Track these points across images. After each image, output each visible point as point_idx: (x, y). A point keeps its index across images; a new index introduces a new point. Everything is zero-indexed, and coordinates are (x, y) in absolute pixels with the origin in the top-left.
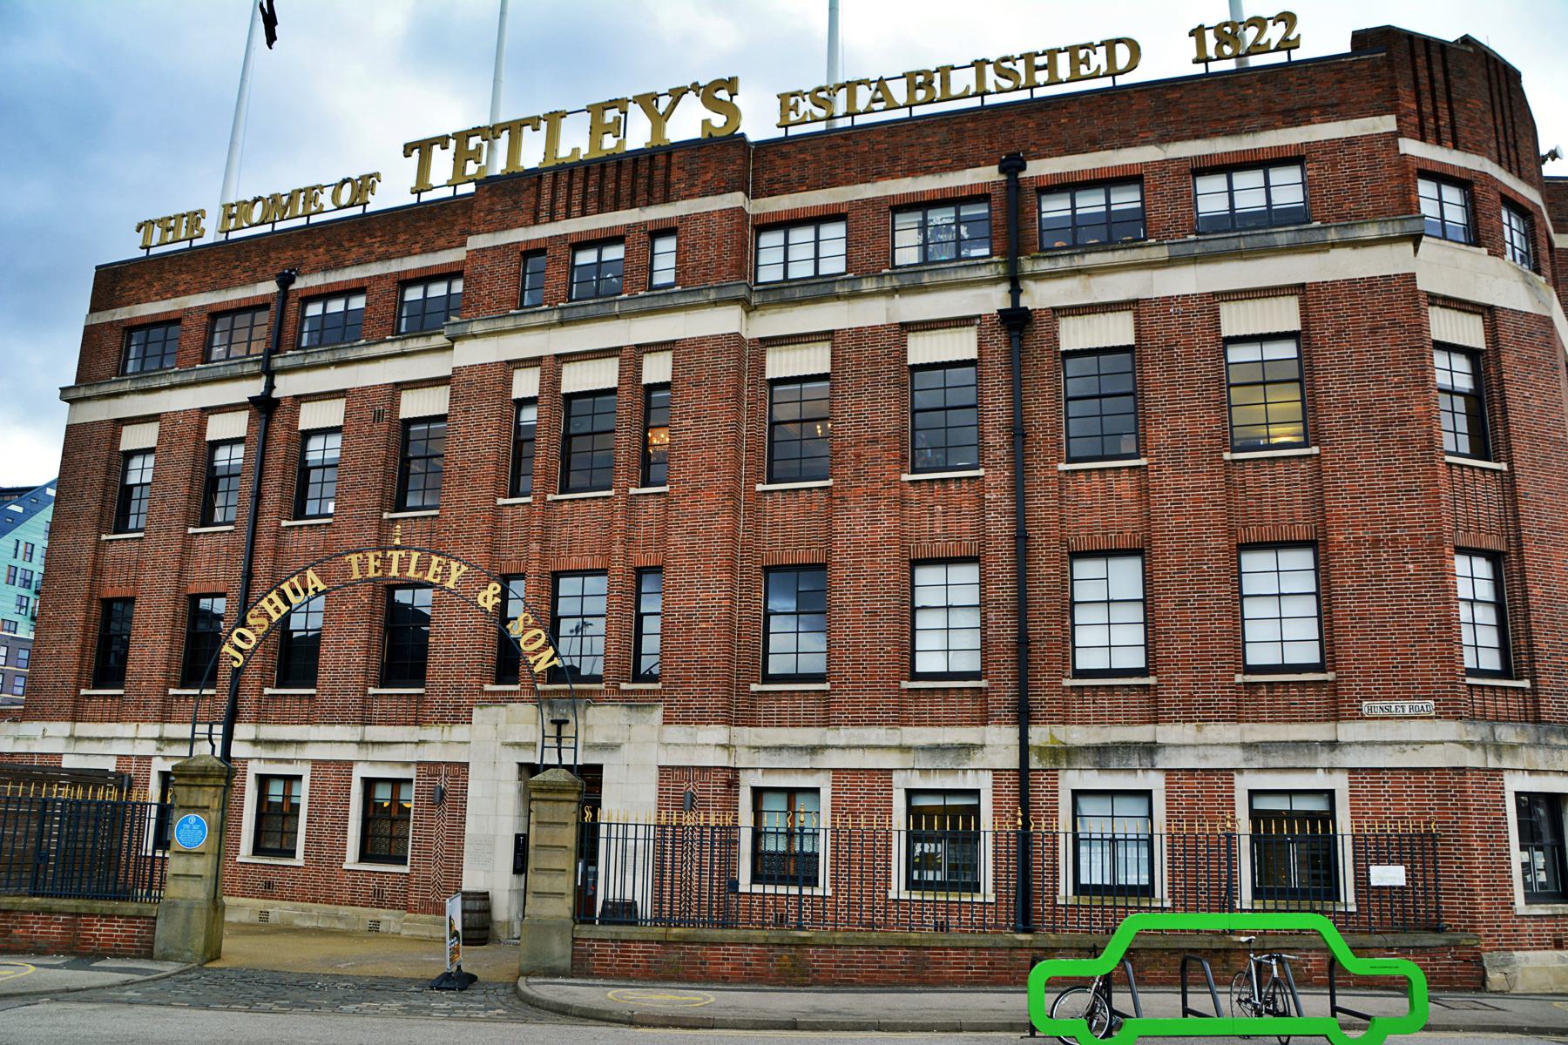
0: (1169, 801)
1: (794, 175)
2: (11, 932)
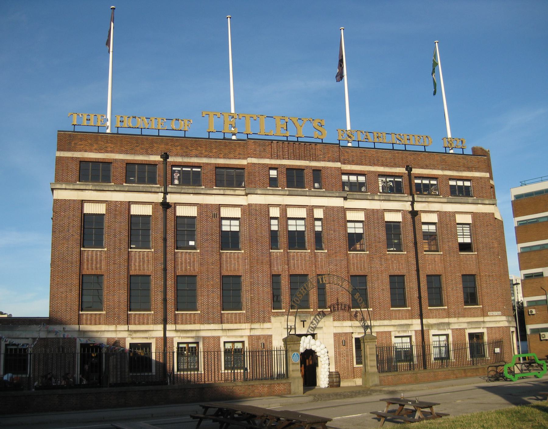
0: (453, 336)
1: (351, 159)
2: (254, 391)
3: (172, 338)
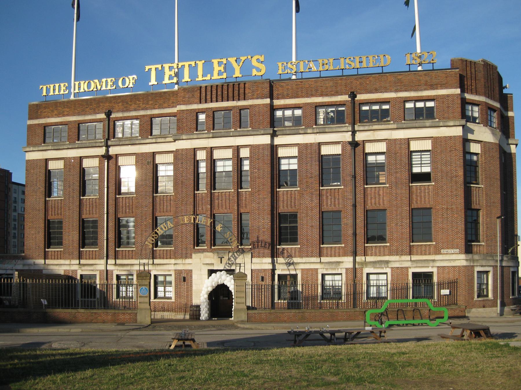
0: (392, 275)
1: (285, 93)
3: (112, 271)
